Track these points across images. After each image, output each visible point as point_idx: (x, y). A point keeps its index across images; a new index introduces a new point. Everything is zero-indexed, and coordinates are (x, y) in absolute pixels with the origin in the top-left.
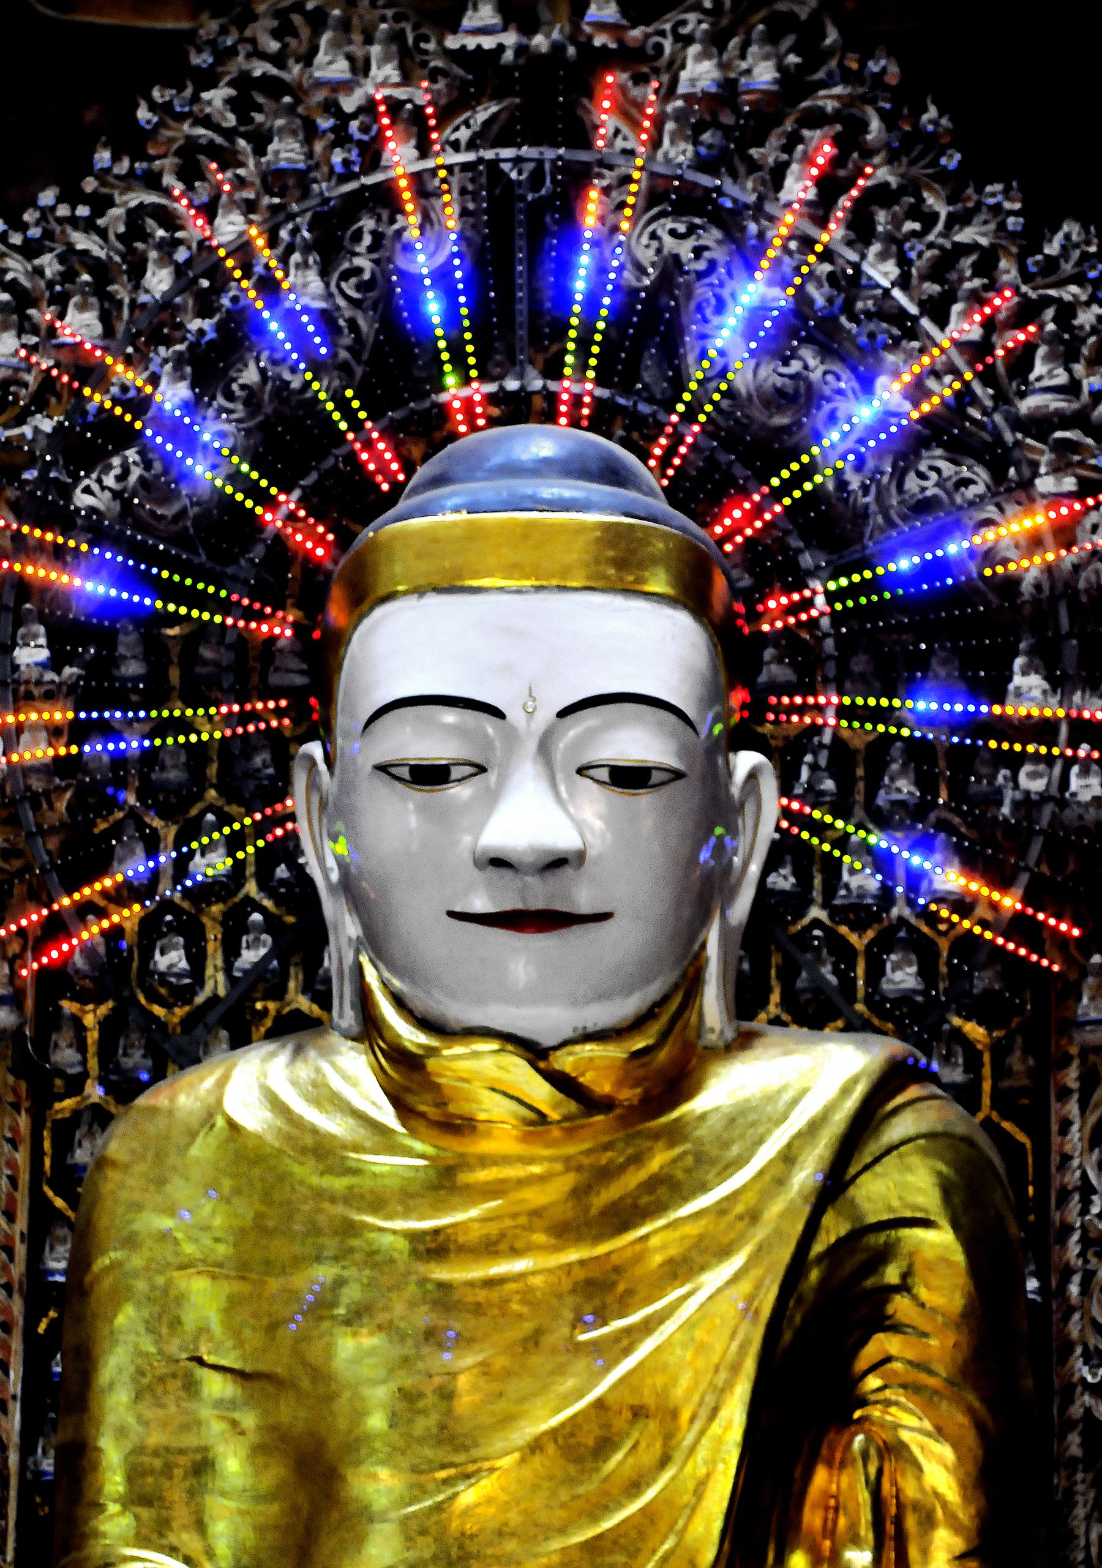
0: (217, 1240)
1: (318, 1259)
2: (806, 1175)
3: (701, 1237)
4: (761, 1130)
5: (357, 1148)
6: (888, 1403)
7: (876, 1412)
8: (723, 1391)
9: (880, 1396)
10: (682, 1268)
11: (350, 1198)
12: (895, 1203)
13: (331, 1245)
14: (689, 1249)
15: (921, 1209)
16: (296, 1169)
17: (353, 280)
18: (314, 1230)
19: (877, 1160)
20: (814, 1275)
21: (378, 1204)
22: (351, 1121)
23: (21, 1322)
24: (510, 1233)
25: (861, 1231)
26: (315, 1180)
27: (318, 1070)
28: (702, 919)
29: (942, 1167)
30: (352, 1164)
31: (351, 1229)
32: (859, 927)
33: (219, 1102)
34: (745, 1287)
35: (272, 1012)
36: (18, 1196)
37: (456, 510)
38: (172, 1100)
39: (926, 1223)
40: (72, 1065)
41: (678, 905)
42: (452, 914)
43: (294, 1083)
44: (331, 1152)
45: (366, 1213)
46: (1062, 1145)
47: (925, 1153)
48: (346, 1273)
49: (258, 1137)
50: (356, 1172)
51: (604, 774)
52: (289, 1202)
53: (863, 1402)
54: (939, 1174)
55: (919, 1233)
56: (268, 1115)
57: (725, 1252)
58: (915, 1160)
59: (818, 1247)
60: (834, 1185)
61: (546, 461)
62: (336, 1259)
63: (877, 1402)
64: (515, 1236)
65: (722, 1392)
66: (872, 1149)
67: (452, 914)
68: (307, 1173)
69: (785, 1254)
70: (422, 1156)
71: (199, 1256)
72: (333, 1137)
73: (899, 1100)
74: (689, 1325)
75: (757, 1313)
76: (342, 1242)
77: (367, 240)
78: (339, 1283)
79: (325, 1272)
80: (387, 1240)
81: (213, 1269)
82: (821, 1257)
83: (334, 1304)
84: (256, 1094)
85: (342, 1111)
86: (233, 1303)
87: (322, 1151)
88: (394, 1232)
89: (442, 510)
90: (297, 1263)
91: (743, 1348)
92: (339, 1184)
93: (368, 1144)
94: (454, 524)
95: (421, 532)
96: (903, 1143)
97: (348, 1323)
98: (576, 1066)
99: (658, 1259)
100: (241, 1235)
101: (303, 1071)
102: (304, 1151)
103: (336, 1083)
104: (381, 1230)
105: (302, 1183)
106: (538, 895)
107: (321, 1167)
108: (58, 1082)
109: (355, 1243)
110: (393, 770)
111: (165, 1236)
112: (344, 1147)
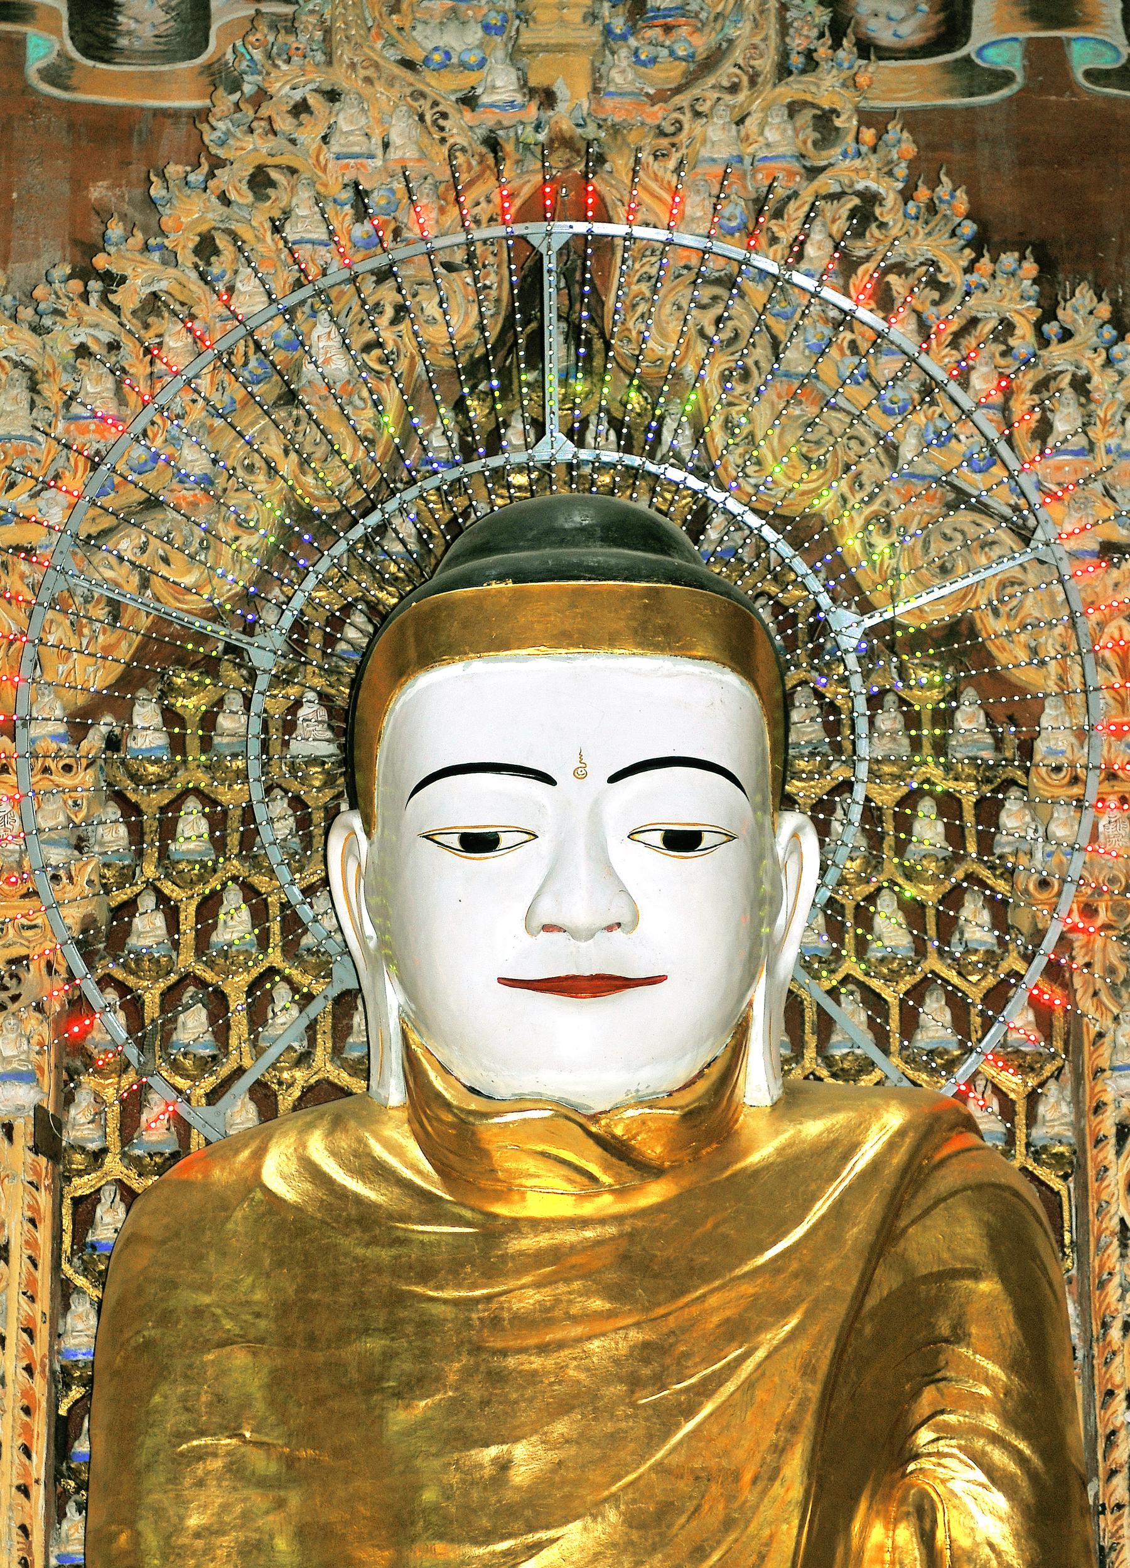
0: (258, 1315)
1: (366, 1331)
2: (858, 1231)
3: (756, 1297)
4: (813, 1186)
5: (405, 1218)
6: (940, 1454)
7: (925, 1463)
8: (783, 1451)
9: (932, 1448)
10: (739, 1330)
11: (398, 1270)
12: (946, 1255)
13: (380, 1318)
14: (746, 1310)
15: (971, 1261)
16: (341, 1240)
17: (376, 352)
18: (362, 1302)
19: (926, 1212)
20: (868, 1330)
21: (426, 1273)
22: (397, 1191)
23: (44, 1404)
24: (564, 1298)
25: (912, 1284)
26: (359, 1251)
27: (360, 1140)
28: (750, 978)
29: (987, 1217)
30: (400, 1234)
31: (400, 1299)
32: (892, 977)
33: (257, 1174)
34: (803, 1345)
35: (300, 1083)
36: (38, 1275)
37: (501, 578)
38: (206, 1175)
39: (975, 1275)
40: (92, 1141)
41: (730, 966)
42: (504, 981)
43: (334, 1153)
44: (377, 1222)
45: (417, 1284)
46: (1099, 1192)
47: (973, 1205)
48: (395, 1345)
49: (297, 1208)
50: (402, 1242)
51: (657, 838)
52: (335, 1274)
53: (916, 1457)
54: (988, 1224)
55: (969, 1283)
56: (308, 1186)
57: (783, 1310)
58: (962, 1211)
59: (871, 1302)
60: (886, 1237)
61: (582, 529)
62: (385, 1331)
63: (929, 1455)
64: (570, 1302)
65: (780, 1450)
66: (922, 1201)
67: (504, 981)
68: (352, 1245)
69: (839, 1311)
70: (469, 1224)
71: (237, 1331)
72: (378, 1206)
73: (945, 1152)
74: (749, 1385)
75: (814, 1370)
76: (391, 1313)
77: (389, 312)
78: (389, 1356)
79: (374, 1345)
80: (438, 1310)
81: (254, 1343)
82: (873, 1314)
83: (381, 1378)
84: (293, 1167)
85: (387, 1180)
86: (277, 1380)
87: (365, 1218)
88: (445, 1301)
89: (487, 579)
90: (343, 1336)
91: (802, 1405)
92: (385, 1255)
93: (415, 1213)
94: (499, 592)
95: (466, 601)
96: (953, 1194)
97: (398, 1395)
98: (627, 1130)
99: (715, 1319)
100: (284, 1309)
101: (344, 1142)
102: (348, 1221)
103: (379, 1151)
104: (432, 1299)
105: (347, 1254)
106: (587, 960)
107: (366, 1237)
108: (78, 1157)
109: (403, 1314)
110: (436, 838)
111: (199, 1312)
112: (391, 1217)
